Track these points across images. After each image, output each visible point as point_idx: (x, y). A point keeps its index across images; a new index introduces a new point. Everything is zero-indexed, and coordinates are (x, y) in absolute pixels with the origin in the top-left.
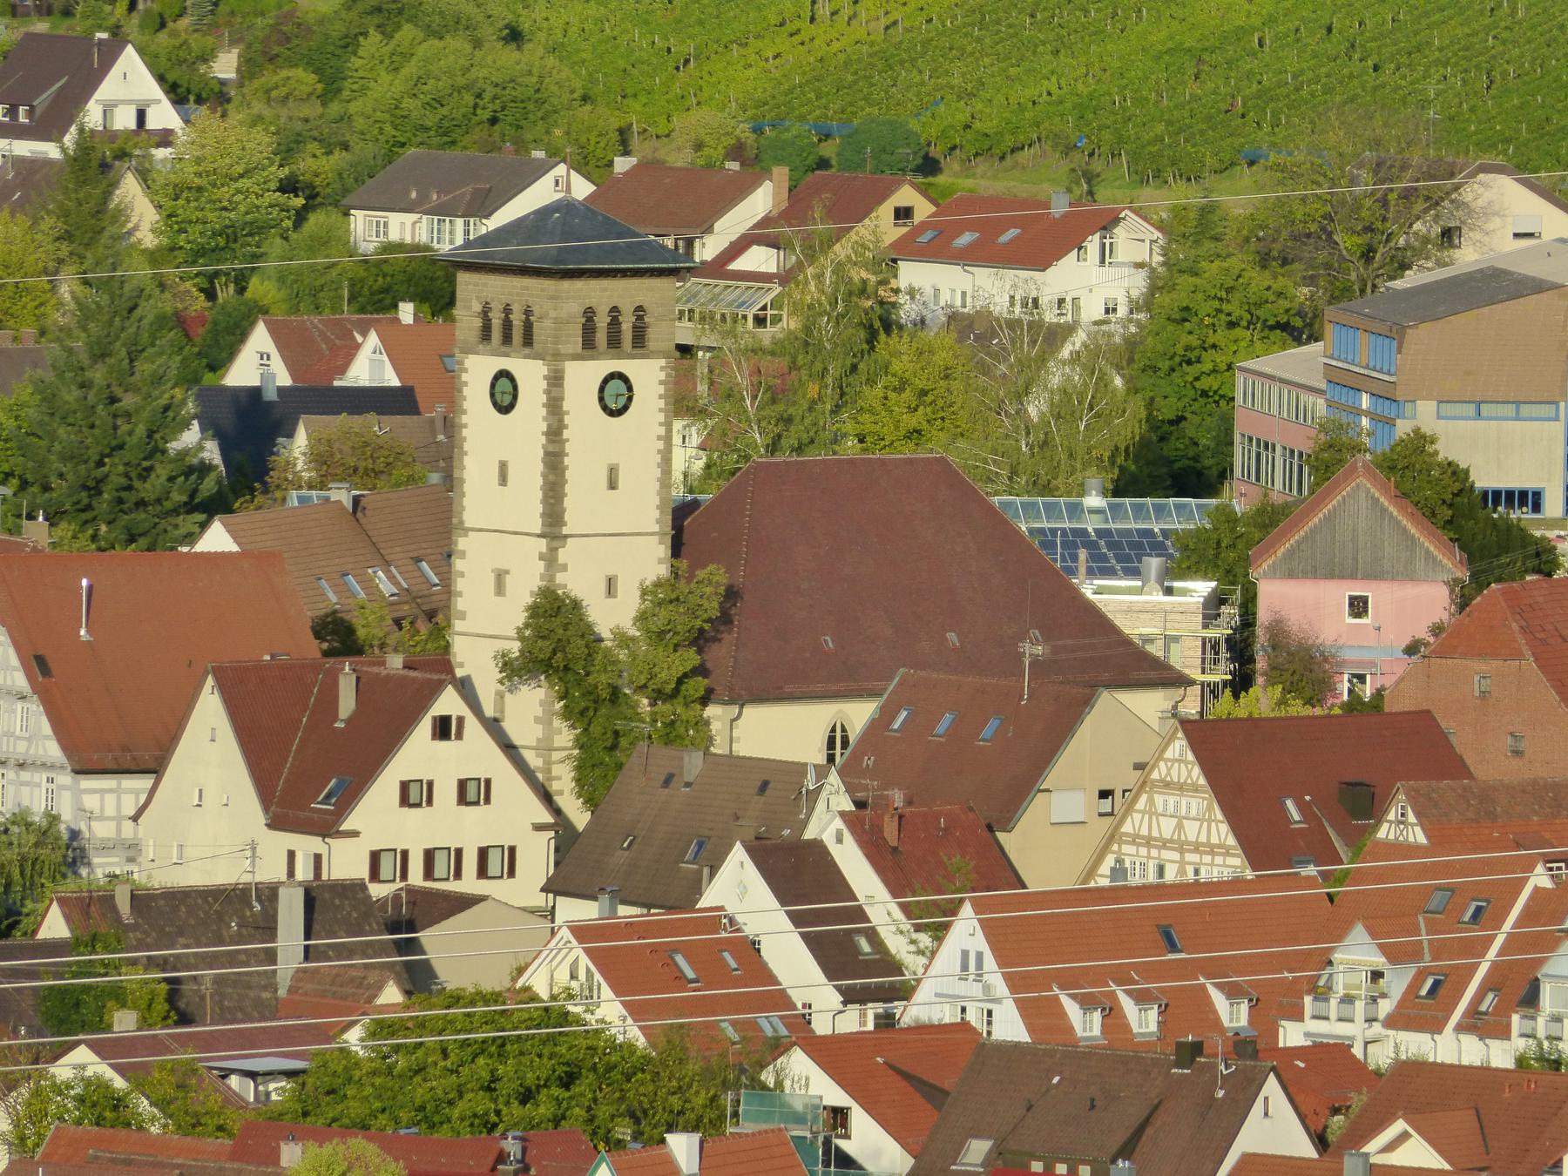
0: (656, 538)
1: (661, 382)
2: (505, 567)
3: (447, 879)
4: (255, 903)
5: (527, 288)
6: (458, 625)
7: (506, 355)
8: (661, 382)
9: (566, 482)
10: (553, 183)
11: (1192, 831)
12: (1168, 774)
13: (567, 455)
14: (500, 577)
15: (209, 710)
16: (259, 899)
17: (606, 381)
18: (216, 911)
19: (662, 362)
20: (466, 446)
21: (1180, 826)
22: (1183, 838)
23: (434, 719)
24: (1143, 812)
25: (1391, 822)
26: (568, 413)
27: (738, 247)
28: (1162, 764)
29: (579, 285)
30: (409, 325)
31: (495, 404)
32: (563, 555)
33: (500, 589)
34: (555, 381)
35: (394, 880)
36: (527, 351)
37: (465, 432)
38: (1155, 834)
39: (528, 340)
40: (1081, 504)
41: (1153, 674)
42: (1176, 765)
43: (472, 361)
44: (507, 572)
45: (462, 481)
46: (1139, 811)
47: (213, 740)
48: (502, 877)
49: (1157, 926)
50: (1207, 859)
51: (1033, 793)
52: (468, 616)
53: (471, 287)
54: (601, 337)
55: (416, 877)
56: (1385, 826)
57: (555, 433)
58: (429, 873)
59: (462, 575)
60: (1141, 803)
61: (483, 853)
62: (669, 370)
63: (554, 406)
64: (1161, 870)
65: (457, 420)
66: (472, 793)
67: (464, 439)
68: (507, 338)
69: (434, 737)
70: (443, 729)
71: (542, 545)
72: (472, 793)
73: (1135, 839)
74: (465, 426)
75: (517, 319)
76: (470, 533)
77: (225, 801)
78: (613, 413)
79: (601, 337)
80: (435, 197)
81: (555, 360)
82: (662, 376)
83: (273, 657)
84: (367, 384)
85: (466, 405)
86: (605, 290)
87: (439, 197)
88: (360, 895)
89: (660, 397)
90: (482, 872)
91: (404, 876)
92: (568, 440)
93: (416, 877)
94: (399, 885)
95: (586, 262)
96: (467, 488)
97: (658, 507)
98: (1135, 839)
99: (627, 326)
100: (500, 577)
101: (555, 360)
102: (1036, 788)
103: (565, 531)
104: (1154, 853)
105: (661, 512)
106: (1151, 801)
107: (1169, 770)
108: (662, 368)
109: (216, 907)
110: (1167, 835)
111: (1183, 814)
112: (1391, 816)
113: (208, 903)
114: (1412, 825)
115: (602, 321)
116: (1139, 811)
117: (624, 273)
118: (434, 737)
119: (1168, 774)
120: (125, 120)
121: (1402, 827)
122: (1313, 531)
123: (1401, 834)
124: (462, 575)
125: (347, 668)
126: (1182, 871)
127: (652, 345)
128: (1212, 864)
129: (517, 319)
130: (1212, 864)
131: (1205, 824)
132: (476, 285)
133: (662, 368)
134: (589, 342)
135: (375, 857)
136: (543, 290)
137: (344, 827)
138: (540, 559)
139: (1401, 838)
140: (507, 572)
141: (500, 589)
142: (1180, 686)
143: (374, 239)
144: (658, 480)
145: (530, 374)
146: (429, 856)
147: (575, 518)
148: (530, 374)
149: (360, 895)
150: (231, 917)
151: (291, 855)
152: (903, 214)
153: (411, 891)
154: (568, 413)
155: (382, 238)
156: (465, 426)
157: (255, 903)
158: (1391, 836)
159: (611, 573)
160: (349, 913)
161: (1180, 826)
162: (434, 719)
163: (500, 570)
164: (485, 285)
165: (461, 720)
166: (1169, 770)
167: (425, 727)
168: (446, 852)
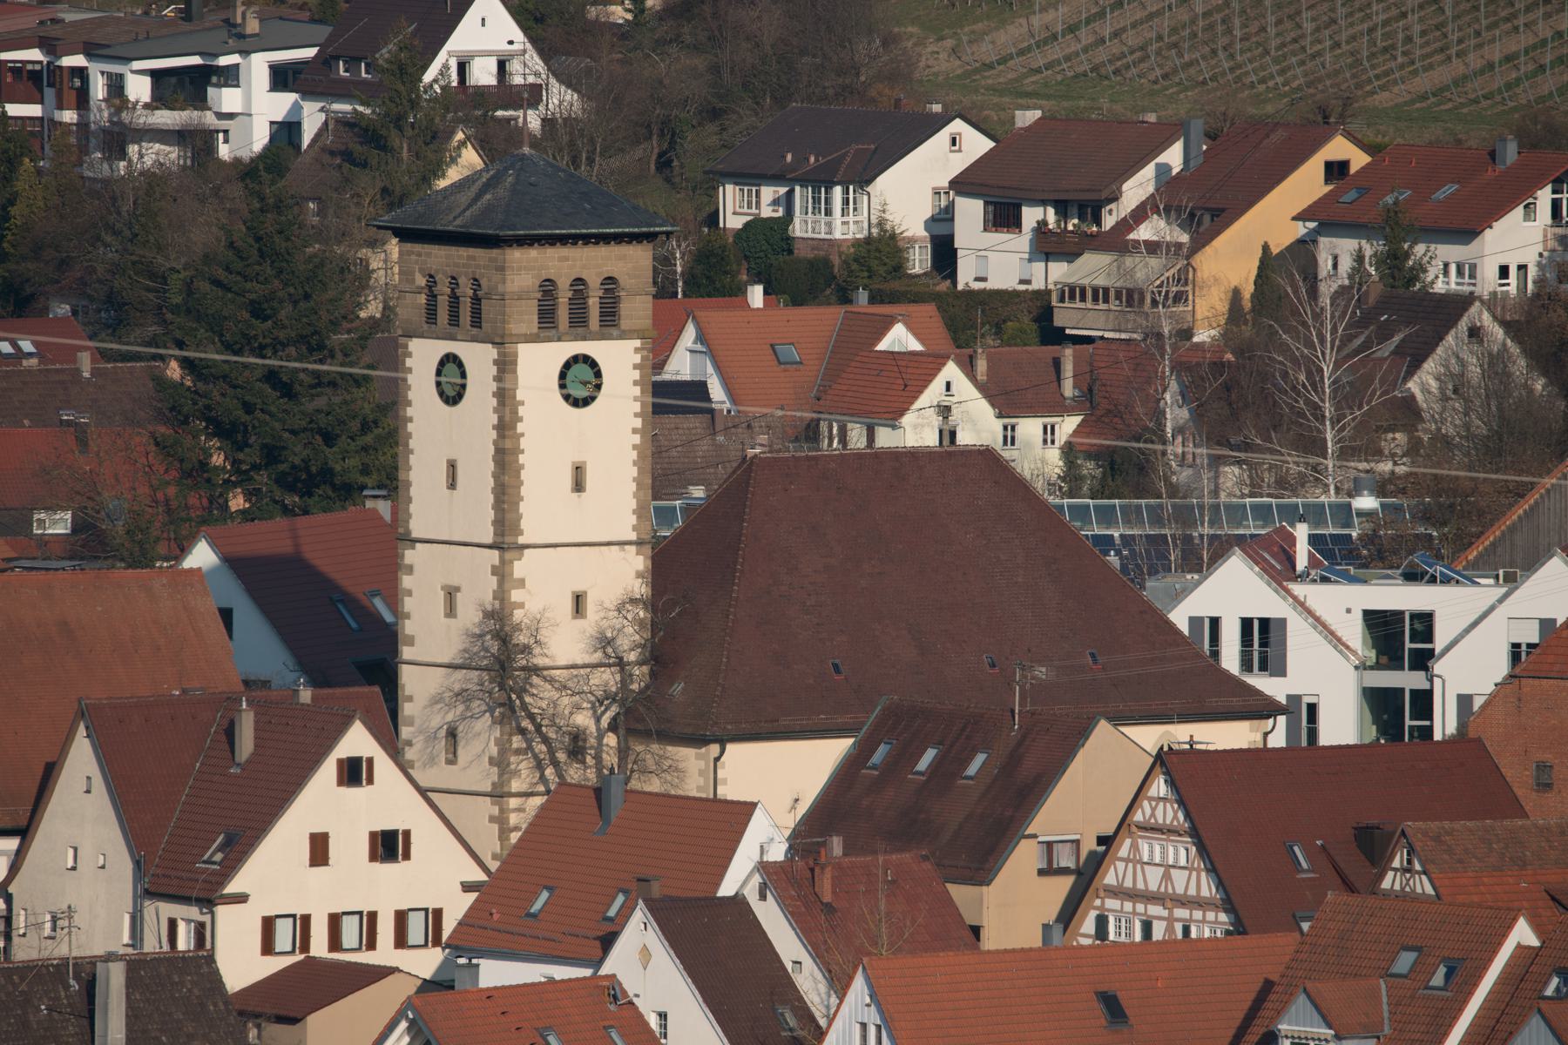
0: (633, 548)
1: (636, 367)
2: (455, 583)
3: (359, 949)
4: (72, 982)
5: (473, 258)
6: (407, 653)
7: (453, 338)
8: (636, 367)
9: (522, 483)
10: (948, 141)
11: (1180, 881)
12: (1153, 815)
13: (522, 452)
14: (451, 593)
15: (81, 759)
16: (77, 977)
17: (567, 365)
18: (22, 992)
19: (637, 343)
20: (412, 444)
21: (1167, 877)
22: (1170, 891)
23: (340, 762)
24: (1127, 860)
25: (1395, 870)
26: (522, 403)
27: (1140, 215)
28: (1146, 803)
29: (533, 253)
30: (758, 309)
31: (441, 394)
32: (519, 569)
33: (451, 611)
34: (505, 367)
35: (293, 952)
36: (580, 330)
37: (410, 427)
38: (1140, 885)
39: (477, 320)
40: (1349, 505)
41: (1236, 702)
42: (1161, 804)
43: (415, 345)
44: (458, 589)
45: (408, 484)
46: (1122, 859)
47: (88, 791)
48: (426, 945)
49: (1096, 993)
50: (1198, 915)
51: (1018, 838)
52: (417, 641)
53: (414, 257)
54: (563, 314)
55: (319, 946)
56: (1390, 874)
57: (506, 426)
58: (335, 943)
59: (410, 593)
60: (1124, 850)
61: (401, 918)
62: (645, 353)
63: (505, 399)
64: (1147, 927)
65: (401, 413)
66: (388, 846)
67: (409, 436)
68: (454, 319)
69: (340, 783)
70: (353, 772)
71: (494, 556)
72: (388, 846)
73: (1118, 892)
74: (411, 420)
75: (466, 290)
76: (526, 552)
77: (101, 862)
78: (579, 403)
79: (563, 314)
80: (812, 159)
81: (500, 340)
82: (637, 359)
83: (184, 691)
84: (688, 378)
85: (411, 395)
86: (567, 259)
87: (817, 160)
88: (205, 969)
89: (635, 383)
90: (401, 941)
91: (305, 947)
92: (522, 435)
93: (319, 946)
94: (299, 957)
95: (540, 226)
96: (413, 491)
97: (634, 512)
98: (1118, 892)
99: (593, 303)
100: (451, 593)
101: (500, 340)
102: (1020, 833)
103: (521, 540)
104: (1140, 908)
105: (639, 518)
106: (1135, 847)
107: (1153, 809)
108: (637, 350)
109: (23, 987)
110: (1153, 887)
111: (1171, 863)
112: (1396, 863)
113: (13, 984)
114: (1418, 872)
115: (443, 288)
116: (1122, 859)
117: (587, 239)
118: (340, 783)
119: (1153, 815)
120: (483, 74)
121: (1408, 875)
122: (1512, 529)
123: (1407, 884)
124: (410, 593)
125: (244, 704)
126: (1170, 929)
127: (625, 324)
128: (1204, 921)
129: (466, 290)
130: (1204, 921)
131: (1194, 873)
132: (419, 255)
133: (637, 350)
134: (547, 316)
135: (268, 924)
136: (491, 260)
137: (473, 896)
138: (493, 574)
139: (1408, 889)
140: (458, 589)
141: (451, 611)
142: (1269, 717)
143: (746, 210)
144: (634, 479)
145: (478, 358)
146: (335, 921)
147: (534, 522)
148: (478, 358)
149: (205, 969)
150: (40, 999)
151: (173, 924)
152: (1336, 170)
153: (312, 962)
154: (522, 403)
155: (754, 211)
156: (411, 420)
157: (72, 982)
158: (1397, 887)
159: (579, 588)
160: (189, 991)
161: (1167, 877)
162: (340, 762)
163: (450, 587)
164: (429, 255)
165: (370, 761)
166: (1153, 809)
167: (328, 771)
168: (290, 920)
